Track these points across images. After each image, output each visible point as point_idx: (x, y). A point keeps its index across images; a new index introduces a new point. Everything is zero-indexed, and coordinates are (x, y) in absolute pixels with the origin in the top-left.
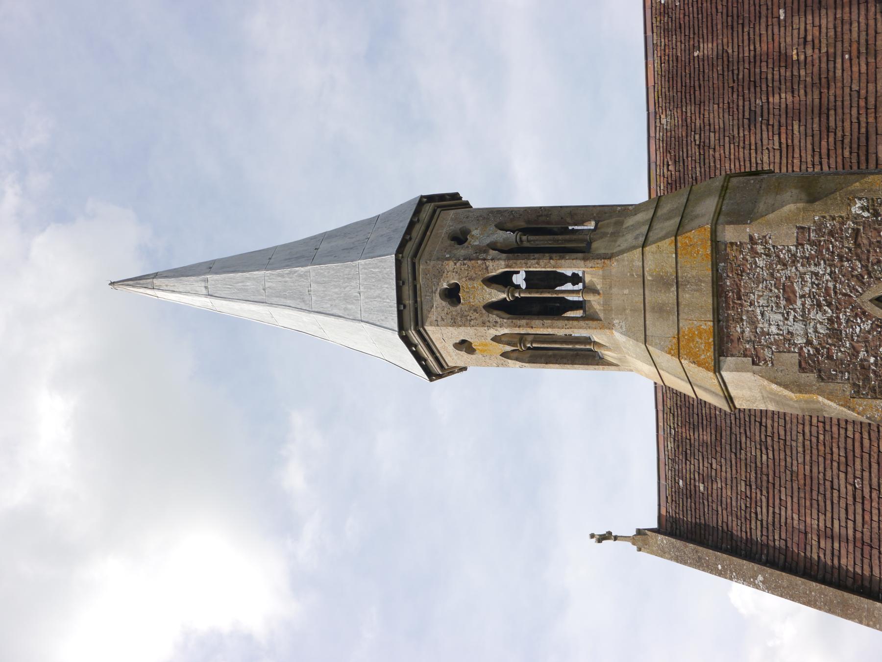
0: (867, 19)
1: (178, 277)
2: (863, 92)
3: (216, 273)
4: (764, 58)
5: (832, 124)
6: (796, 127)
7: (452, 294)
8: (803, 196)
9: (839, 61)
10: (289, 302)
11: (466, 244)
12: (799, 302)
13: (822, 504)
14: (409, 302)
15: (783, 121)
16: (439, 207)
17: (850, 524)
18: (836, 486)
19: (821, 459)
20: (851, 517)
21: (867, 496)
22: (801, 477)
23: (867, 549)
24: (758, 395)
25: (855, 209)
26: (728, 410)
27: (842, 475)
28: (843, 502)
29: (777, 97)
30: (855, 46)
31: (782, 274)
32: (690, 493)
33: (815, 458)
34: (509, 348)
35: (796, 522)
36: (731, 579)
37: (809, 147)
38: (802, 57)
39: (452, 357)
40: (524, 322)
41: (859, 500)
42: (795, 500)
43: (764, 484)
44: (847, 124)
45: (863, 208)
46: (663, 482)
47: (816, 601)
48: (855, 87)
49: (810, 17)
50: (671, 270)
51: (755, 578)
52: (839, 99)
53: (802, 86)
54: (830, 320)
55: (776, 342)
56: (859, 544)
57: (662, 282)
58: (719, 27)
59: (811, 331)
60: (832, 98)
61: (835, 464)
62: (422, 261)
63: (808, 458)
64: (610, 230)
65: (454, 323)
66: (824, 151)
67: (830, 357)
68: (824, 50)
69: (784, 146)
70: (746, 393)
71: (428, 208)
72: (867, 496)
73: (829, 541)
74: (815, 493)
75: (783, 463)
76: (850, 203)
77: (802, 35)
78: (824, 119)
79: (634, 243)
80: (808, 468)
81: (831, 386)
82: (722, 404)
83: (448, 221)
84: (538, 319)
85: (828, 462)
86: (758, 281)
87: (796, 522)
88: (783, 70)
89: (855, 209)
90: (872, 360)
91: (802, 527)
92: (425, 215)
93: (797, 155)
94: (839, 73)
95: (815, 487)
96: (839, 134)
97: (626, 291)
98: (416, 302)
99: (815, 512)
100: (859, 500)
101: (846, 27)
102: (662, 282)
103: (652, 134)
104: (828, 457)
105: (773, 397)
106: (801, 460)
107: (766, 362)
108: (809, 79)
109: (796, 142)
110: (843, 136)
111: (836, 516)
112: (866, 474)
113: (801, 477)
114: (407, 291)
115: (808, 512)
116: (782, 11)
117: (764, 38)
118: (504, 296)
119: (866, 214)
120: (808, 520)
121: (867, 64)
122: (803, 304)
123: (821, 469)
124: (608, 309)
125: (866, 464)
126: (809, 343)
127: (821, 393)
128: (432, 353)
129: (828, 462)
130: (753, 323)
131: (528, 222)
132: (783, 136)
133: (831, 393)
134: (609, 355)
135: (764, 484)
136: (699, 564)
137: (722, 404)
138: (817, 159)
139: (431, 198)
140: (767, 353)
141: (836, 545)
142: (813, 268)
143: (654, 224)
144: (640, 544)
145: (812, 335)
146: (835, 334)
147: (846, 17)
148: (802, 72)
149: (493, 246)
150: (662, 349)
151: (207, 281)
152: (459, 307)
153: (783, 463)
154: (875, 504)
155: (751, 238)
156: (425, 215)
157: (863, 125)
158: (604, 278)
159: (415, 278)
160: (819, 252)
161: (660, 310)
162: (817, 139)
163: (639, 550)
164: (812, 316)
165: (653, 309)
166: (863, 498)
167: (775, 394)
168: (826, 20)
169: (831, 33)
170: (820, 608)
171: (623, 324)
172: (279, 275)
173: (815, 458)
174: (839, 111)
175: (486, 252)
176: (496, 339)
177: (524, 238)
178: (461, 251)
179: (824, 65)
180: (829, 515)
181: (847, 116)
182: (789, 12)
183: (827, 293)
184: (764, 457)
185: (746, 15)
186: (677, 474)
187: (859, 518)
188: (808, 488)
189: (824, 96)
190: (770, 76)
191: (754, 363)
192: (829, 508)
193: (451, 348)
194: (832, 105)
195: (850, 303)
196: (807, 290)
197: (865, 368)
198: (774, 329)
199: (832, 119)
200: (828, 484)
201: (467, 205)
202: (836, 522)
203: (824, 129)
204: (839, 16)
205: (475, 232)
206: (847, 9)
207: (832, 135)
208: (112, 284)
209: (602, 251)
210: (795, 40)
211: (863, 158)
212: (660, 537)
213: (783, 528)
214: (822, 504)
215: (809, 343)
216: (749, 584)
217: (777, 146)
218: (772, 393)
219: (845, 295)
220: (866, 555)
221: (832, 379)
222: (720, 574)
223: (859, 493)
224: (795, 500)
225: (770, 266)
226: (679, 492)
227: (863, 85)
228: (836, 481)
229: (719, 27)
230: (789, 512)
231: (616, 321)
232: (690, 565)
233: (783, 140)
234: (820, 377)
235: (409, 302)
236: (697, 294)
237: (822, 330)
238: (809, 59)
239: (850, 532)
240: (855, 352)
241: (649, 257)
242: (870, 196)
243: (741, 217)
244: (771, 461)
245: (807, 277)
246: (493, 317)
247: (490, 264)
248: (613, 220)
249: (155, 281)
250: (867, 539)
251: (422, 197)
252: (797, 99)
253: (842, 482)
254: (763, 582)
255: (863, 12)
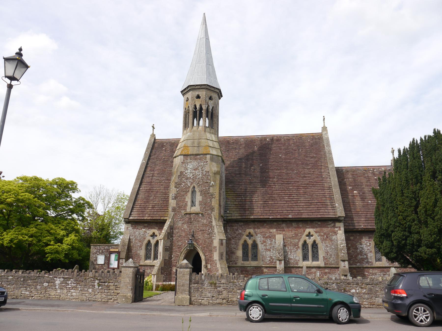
0: (257, 182)
1: (205, 31)
2: (243, 182)
3: (206, 40)
4: (253, 161)
5: (237, 176)
6: (237, 168)
7: (198, 97)
8: (215, 172)
9: (250, 177)
10: (198, 58)
11: (209, 100)
12: (194, 171)
13: (159, 174)
14: (197, 87)
15: (239, 166)
16: (218, 93)
17: (155, 180)
18: (163, 177)
19: (168, 174)
20: (156, 180)
21: (161, 184)
22: (165, 170)
23: (150, 183)
24: (176, 163)
25: (212, 182)
26: (174, 157)
27: (165, 178)
28: (159, 179)
29: (244, 164)
30: (252, 180)
31: (200, 168)
32: (163, 146)
33: (169, 173)
34: (187, 109)
35: (156, 169)
36: (144, 155)
37: (233, 171)
38: (251, 169)
39: (186, 96)
40: (192, 113)
41: (160, 182)
42: (160, 169)
43: (164, 162)
44: (237, 179)
45: (212, 184)
46: (165, 140)
47: (139, 173)
48: (244, 180)
49: (259, 171)
50: (201, 145)
51: (144, 161)
52: (242, 177)
53: (246, 169)
54: (190, 178)
55: (186, 167)
56: (151, 182)
57: (199, 143)
58: (260, 152)
59: (188, 174)
60: (242, 176)
61: (167, 177)
62: (205, 90)
63: (169, 171)
64: (211, 132)
65: (192, 98)
66: (232, 174)
67: (183, 177)
68: (252, 174)
69: (234, 166)
70: (176, 161)
71: (218, 91)
72: (161, 184)
73: (152, 176)
74: (162, 173)
75: (168, 166)
76: (213, 182)
77: (256, 169)
78: (238, 174)
79: (208, 137)
80: (167, 171)
81: (177, 178)
82: (174, 156)
83: (215, 96)
84: (193, 116)
85: (168, 175)
86: (199, 163)
87: (156, 169)
88: (249, 165)
89: (212, 182)
90: (182, 186)
91: (155, 170)
92: (216, 90)
93: (232, 168)
94: (247, 177)
95: (163, 173)
96: (235, 177)
97: (198, 135)
98: (197, 89)
99: (158, 173)
100: (160, 182)
101: (256, 178)
102: (199, 143)
103: (240, 137)
104: (169, 176)
105: (175, 166)
106: (168, 170)
107: (182, 165)
108: (247, 171)
109: (234, 168)
110: (235, 178)
111: (157, 177)
112: (165, 183)
113: (165, 170)
114: (199, 87)
115: (158, 171)
116: (262, 165)
117: (257, 161)
118: (198, 108)
119: (211, 184)
120: (156, 171)
121: (248, 183)
122: (194, 172)
123: (166, 174)
124: (194, 131)
125: (167, 183)
126: (186, 173)
127: (176, 176)
128: (186, 92)
129: (168, 175)
130: (190, 162)
131: (214, 113)
132: (236, 166)
133: (176, 178)
134: (185, 131)
135: (164, 162)
136: (147, 148)
137: (174, 156)
138: (230, 173)
139: (220, 91)
140: (184, 165)
141: (151, 177)
142: (201, 174)
143: (212, 141)
144: (152, 135)
145: (188, 174)
146: (187, 179)
147: (258, 178)
148: (248, 169)
149: (208, 106)
150: (185, 143)
151: (204, 38)
152: (195, 99)
153: (168, 166)
154: (159, 185)
155: (207, 162)
156: (216, 90)
157: (236, 182)
158: (201, 131)
159: (202, 88)
160: (204, 175)
161: (193, 143)
162: (234, 173)
163: (151, 135)
164: (191, 174)
165: (193, 141)
166: (160, 183)
167: (176, 167)
168: (258, 174)
169: (256, 175)
170: (138, 174)
171: (191, 135)
172: (204, 56)
173: (169, 173)
174: (239, 177)
175: (207, 104)
176: (189, 107)
177: (210, 113)
178: (207, 99)
179: (249, 174)
180: (157, 176)
181: (238, 179)
182: (262, 166)
183: (196, 177)
184: (169, 162)
185: (262, 157)
186: (167, 143)
187: (156, 182)
188: (163, 171)
189: (243, 174)
190: (248, 163)
191: (182, 162)
192: (159, 176)
193: (187, 96)
194: (241, 176)
195: (194, 181)
196: (196, 173)
197: (181, 184)
198: (189, 166)
199: (238, 176)
200: (163, 175)
201: (220, 99)
202: (155, 177)
203: (236, 174)
204: (259, 177)
205: (212, 101)
206: (260, 178)
207: (235, 176)
208: (204, 14)
209: (206, 130)
210: (255, 168)
211: (229, 182)
212: (153, 140)
213: (155, 166)
214: (159, 174)
215: (186, 173)
216: (143, 159)
217: (234, 164)
218: (176, 166)
219: (195, 181)
220: (149, 183)
221: (179, 178)
222: (145, 153)
223: (161, 182)
224: (160, 169)
225: (201, 165)
226: (163, 144)
227: (244, 182)
228: (164, 177)
229: (260, 152)
230: (158, 167)
231: (191, 133)
232: (147, 146)
233: (235, 166)
234: (179, 176)
235: (197, 87)
236: (196, 150)
237: (188, 176)
238: (251, 171)
239: (153, 180)
240: (184, 182)
241: (205, 140)
242: (215, 185)
243: (212, 160)
244: (168, 163)
245: (199, 173)
246: (193, 106)
247: (204, 105)
248: (213, 132)
249: (205, 25)
250: (152, 183)
251: (220, 89)
252: (243, 168)
253: (164, 178)
254: (143, 162)
255: (259, 182)
